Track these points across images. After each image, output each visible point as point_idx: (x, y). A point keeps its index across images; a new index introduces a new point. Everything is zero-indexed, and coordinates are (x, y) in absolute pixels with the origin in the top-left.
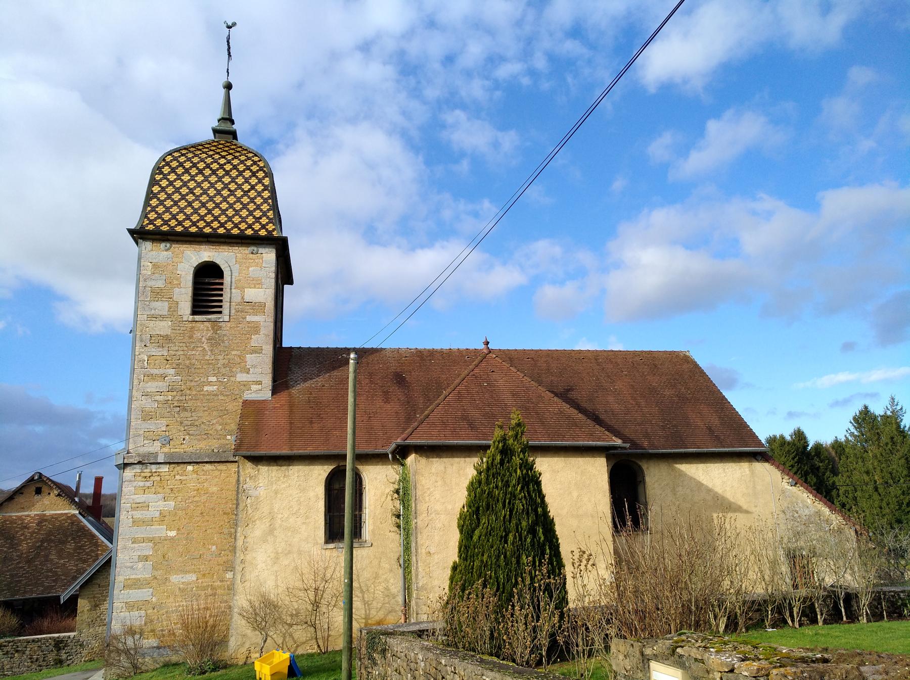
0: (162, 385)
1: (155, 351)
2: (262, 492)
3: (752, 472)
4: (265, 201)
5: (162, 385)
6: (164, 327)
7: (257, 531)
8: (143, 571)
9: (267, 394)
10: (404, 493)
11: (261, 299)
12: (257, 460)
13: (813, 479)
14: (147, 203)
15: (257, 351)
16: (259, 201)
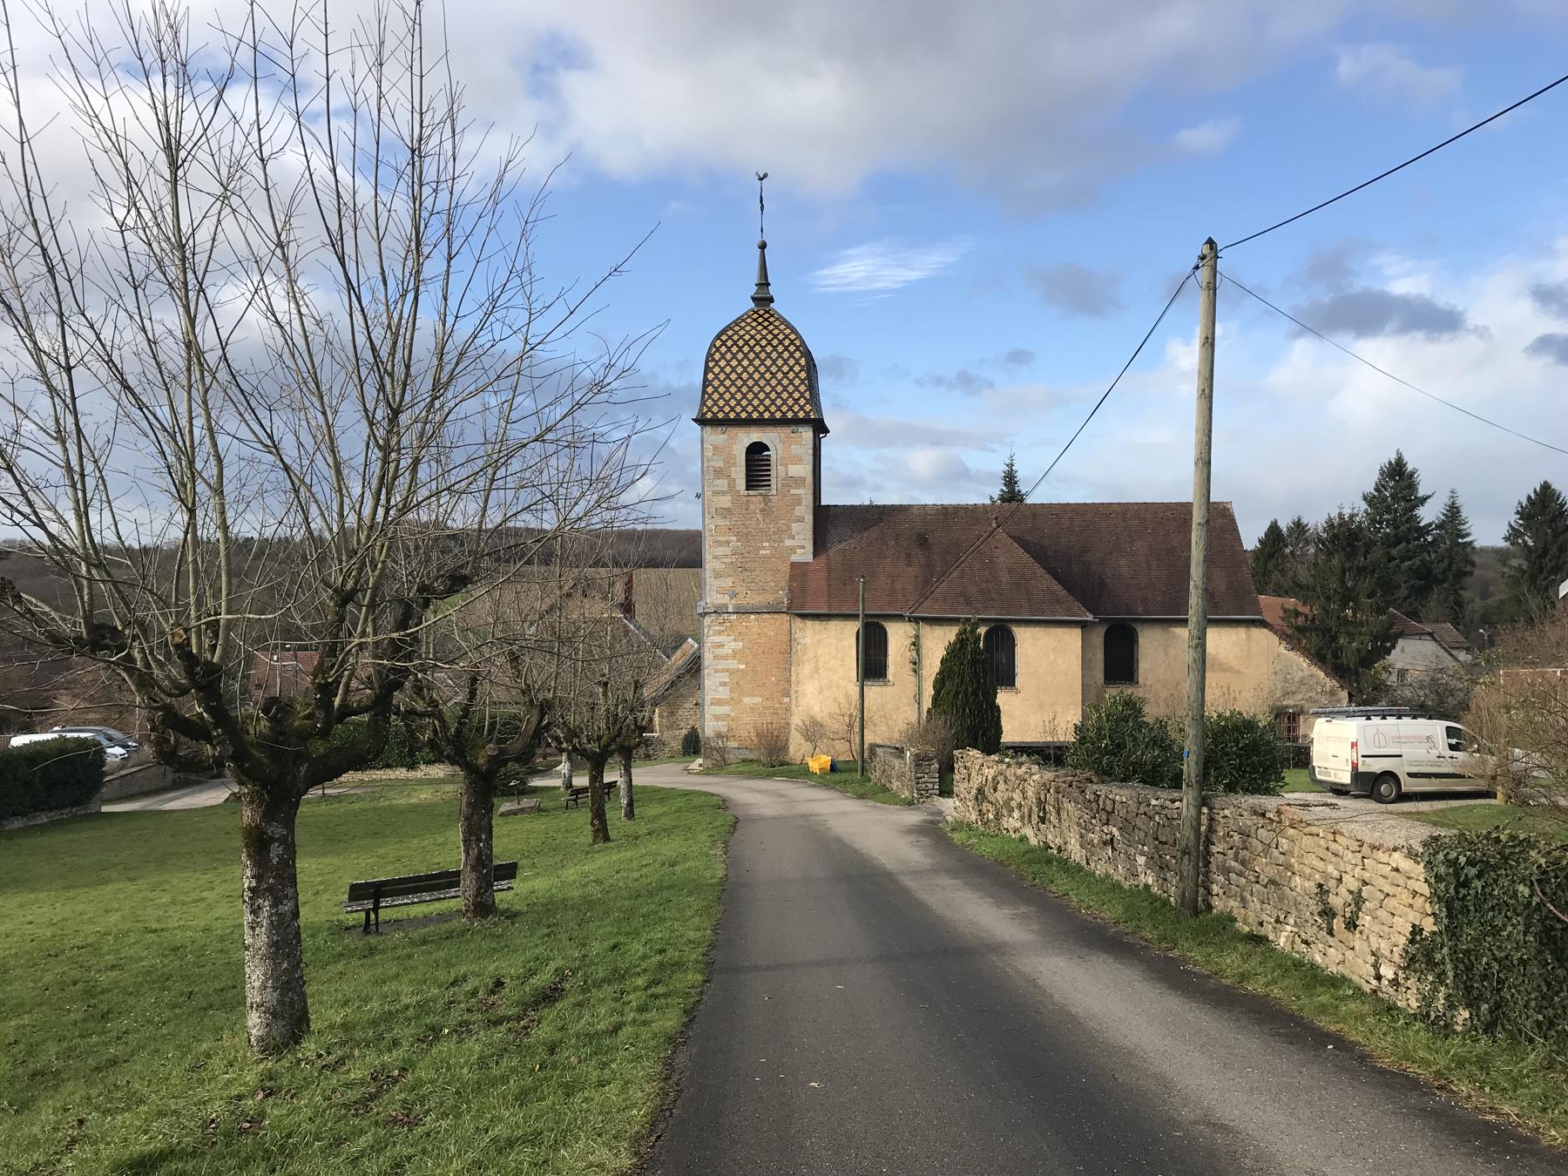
0: (728, 550)
1: (719, 522)
2: (808, 640)
3: (1249, 637)
4: (802, 382)
5: (728, 550)
6: (725, 502)
7: (806, 669)
8: (723, 693)
9: (809, 558)
10: (916, 644)
11: (802, 474)
12: (804, 616)
13: (1316, 641)
14: (704, 392)
15: (801, 520)
16: (797, 382)
